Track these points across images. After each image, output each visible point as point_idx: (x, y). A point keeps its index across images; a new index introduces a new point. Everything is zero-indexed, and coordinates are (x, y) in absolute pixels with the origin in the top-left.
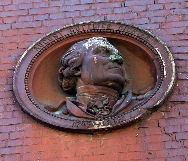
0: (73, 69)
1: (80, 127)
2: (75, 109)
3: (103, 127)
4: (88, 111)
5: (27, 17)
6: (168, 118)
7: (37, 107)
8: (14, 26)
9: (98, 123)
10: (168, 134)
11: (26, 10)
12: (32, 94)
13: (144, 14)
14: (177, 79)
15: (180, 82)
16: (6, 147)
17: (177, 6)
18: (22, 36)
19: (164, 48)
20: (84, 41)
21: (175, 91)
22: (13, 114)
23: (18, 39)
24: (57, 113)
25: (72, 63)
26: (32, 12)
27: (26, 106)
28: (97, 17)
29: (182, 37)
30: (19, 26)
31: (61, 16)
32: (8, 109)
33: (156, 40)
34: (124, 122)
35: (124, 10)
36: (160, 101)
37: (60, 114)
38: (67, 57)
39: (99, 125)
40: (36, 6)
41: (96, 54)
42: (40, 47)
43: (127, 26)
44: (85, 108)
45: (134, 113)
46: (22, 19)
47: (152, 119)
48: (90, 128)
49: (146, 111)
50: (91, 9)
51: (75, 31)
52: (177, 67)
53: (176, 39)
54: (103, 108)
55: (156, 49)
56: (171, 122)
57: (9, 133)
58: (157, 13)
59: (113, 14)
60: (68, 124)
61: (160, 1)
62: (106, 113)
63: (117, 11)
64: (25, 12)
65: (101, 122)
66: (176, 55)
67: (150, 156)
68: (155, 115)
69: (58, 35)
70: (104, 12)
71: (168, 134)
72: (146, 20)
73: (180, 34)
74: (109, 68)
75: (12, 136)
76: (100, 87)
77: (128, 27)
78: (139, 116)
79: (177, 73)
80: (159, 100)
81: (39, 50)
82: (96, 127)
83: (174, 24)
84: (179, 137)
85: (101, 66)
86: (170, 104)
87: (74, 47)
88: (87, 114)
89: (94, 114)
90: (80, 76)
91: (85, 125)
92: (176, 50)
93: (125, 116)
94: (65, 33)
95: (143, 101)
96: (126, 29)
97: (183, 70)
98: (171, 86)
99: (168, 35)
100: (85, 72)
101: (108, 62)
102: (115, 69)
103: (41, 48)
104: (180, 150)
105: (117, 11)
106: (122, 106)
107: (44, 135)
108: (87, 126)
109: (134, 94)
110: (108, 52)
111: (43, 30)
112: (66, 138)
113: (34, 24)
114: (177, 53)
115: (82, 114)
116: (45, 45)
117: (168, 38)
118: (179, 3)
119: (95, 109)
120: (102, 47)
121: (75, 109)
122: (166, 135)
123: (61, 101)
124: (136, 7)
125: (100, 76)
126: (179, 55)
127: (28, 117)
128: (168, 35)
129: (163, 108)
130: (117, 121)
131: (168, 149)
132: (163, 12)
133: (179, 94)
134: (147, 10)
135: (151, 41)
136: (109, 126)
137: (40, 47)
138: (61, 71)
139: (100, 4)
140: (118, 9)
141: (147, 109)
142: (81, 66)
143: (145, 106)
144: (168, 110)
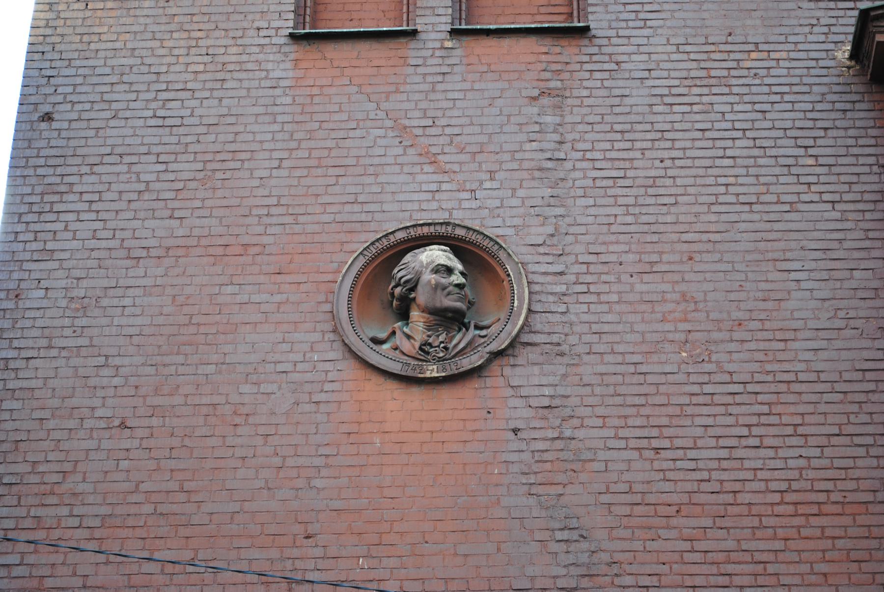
0: (406, 290)
1: (410, 373)
2: (406, 345)
3: (437, 375)
4: (420, 349)
5: (355, 205)
6: (514, 366)
7: (361, 339)
8: (339, 218)
9: (431, 368)
10: (512, 387)
11: (353, 195)
12: (355, 320)
13: (497, 211)
14: (530, 311)
15: (533, 315)
16: (322, 391)
17: (539, 202)
18: (348, 234)
19: (518, 266)
20: (422, 249)
21: (525, 327)
22: (332, 345)
23: (343, 237)
24: (386, 346)
25: (407, 282)
26: (361, 199)
27: (348, 338)
28: (441, 211)
29: (542, 250)
30: (345, 217)
31: (396, 207)
32: (326, 339)
33: (509, 254)
34: (462, 370)
35: (474, 204)
36: (506, 343)
37: (387, 349)
38: (401, 273)
39: (432, 371)
40: (367, 190)
41: (436, 273)
42: (368, 254)
43: (475, 231)
44: (417, 345)
45: (474, 358)
46: (348, 208)
47: (495, 367)
48: (422, 376)
49: (488, 355)
50: (433, 199)
51: (413, 233)
52: (530, 293)
53: (534, 252)
54: (438, 346)
55: (508, 267)
56: (518, 370)
57: (327, 372)
58: (514, 212)
59: (460, 208)
60: (396, 368)
61: (590, 2)
62: (441, 355)
63: (466, 204)
64: (351, 198)
65: (435, 367)
66: (530, 276)
67: (489, 415)
68: (496, 362)
69: (391, 237)
70: (449, 205)
71: (512, 387)
72: (498, 222)
73: (539, 245)
74: (449, 294)
75: (331, 376)
76: (437, 318)
77: (475, 233)
78: (480, 363)
79: (529, 304)
80: (503, 343)
81: (367, 258)
82: (428, 374)
83: (533, 230)
84: (524, 392)
85: (439, 292)
86: (518, 346)
87: (408, 258)
88: (420, 354)
89: (428, 353)
90: (414, 299)
91: (415, 370)
92: (531, 268)
93: (464, 361)
94: (400, 235)
95: (486, 339)
96: (474, 235)
97: (538, 297)
98: (520, 323)
99: (525, 245)
100: (422, 296)
101: (448, 287)
102: (455, 297)
103: (370, 255)
104: (524, 410)
105: (466, 204)
106: (461, 346)
107: (367, 378)
108: (419, 371)
109: (477, 327)
110: (449, 270)
111: (373, 226)
112: (392, 386)
113: (363, 217)
114: (533, 273)
115: (413, 352)
116: (374, 251)
117: (524, 249)
118: (543, 198)
119: (428, 347)
120: (443, 265)
121: (406, 345)
122: (510, 389)
123: (390, 330)
124: (489, 201)
125: (438, 305)
126: (536, 275)
127: (335, 48)
128: (525, 245)
129: (510, 352)
130: (454, 367)
131: (510, 408)
132: (521, 211)
133: (531, 332)
134: (502, 206)
135: (502, 255)
136: (444, 374)
137: (368, 254)
138: (392, 289)
139: (445, 193)
140: (466, 202)
141: (491, 353)
142: (416, 286)
143: (488, 349)
144: (515, 354)
